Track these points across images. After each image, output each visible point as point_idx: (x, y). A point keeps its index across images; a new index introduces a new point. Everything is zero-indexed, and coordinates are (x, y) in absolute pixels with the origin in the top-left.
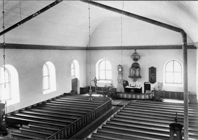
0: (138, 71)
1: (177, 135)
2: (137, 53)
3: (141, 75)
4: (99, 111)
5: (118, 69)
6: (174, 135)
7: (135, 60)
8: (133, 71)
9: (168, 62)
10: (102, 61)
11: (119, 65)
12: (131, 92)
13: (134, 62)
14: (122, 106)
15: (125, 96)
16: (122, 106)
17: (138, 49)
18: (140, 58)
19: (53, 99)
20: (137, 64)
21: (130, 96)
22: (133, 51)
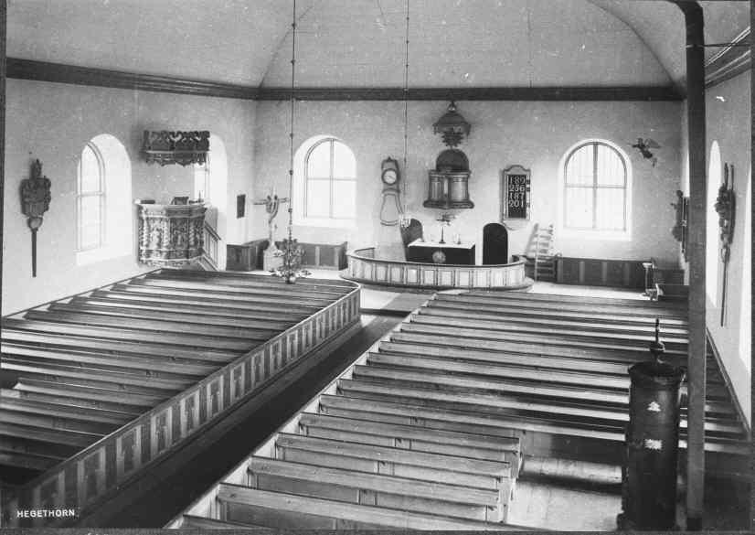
0: (460, 180)
1: (660, 408)
2: (459, 112)
3: (471, 199)
4: (314, 331)
5: (380, 173)
6: (650, 409)
7: (452, 138)
8: (442, 183)
9: (577, 149)
10: (318, 144)
11: (386, 158)
12: (435, 260)
13: (449, 148)
14: (403, 314)
15: (412, 275)
16: (403, 314)
17: (461, 98)
18: (468, 134)
19: (118, 287)
20: (461, 155)
21: (429, 276)
22: (440, 107)
